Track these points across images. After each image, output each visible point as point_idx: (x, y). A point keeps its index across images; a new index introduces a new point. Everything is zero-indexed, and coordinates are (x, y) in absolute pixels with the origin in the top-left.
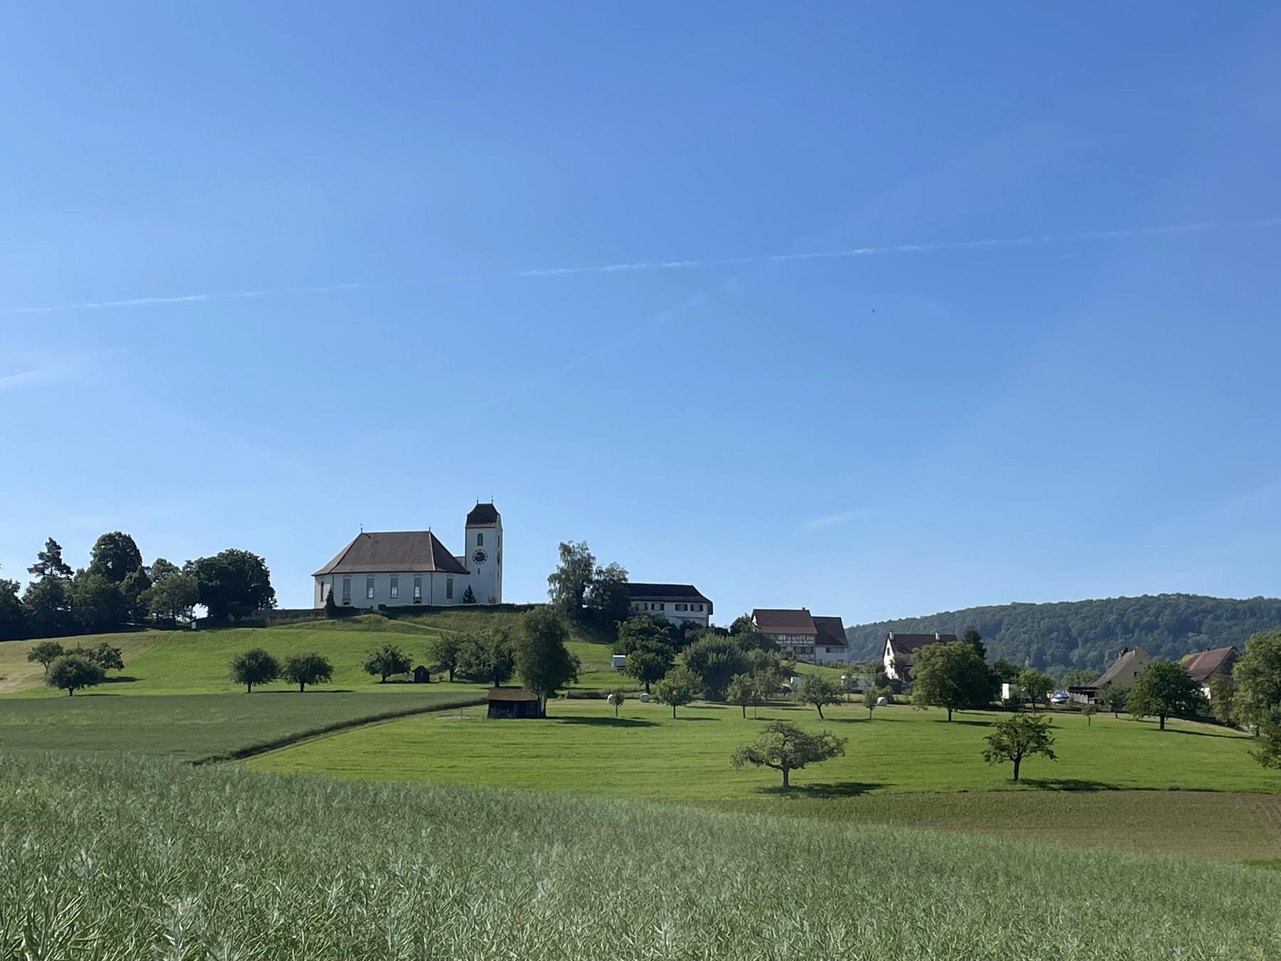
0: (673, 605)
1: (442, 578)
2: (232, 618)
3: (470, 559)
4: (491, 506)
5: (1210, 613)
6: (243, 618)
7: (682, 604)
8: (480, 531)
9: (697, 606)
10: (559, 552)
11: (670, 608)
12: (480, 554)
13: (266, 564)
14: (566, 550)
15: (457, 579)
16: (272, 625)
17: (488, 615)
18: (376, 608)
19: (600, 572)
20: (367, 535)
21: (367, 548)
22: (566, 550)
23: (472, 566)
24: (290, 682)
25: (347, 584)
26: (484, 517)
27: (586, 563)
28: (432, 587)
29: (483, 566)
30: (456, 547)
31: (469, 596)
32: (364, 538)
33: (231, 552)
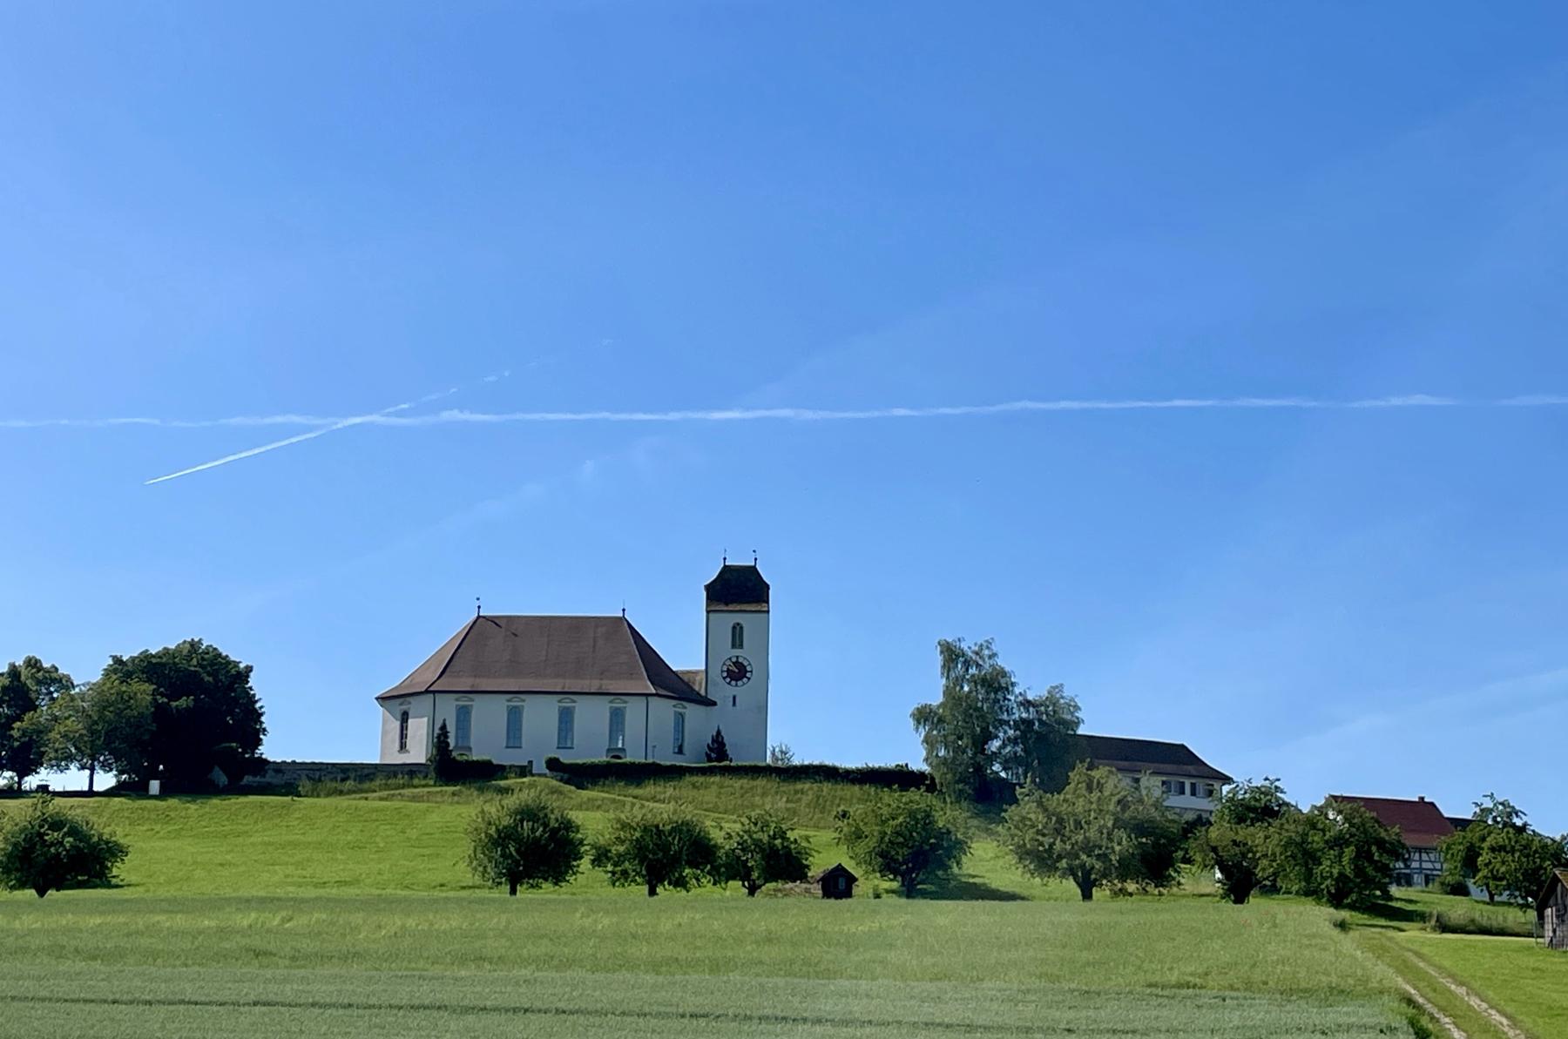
0: (1157, 781)
1: (664, 709)
2: (222, 779)
3: (716, 674)
4: (753, 570)
5: (1347, 843)
6: (247, 779)
7: (1173, 779)
8: (738, 618)
9: (1201, 785)
10: (938, 660)
11: (1151, 785)
12: (736, 664)
13: (253, 681)
14: (951, 655)
15: (692, 711)
16: (314, 793)
17: (785, 787)
18: (540, 766)
19: (1027, 704)
20: (493, 620)
21: (495, 651)
22: (951, 655)
23: (722, 691)
24: (12, 888)
25: (463, 714)
26: (738, 590)
27: (996, 684)
28: (649, 729)
29: (742, 690)
30: (684, 645)
31: (718, 748)
32: (484, 629)
33: (194, 645)
